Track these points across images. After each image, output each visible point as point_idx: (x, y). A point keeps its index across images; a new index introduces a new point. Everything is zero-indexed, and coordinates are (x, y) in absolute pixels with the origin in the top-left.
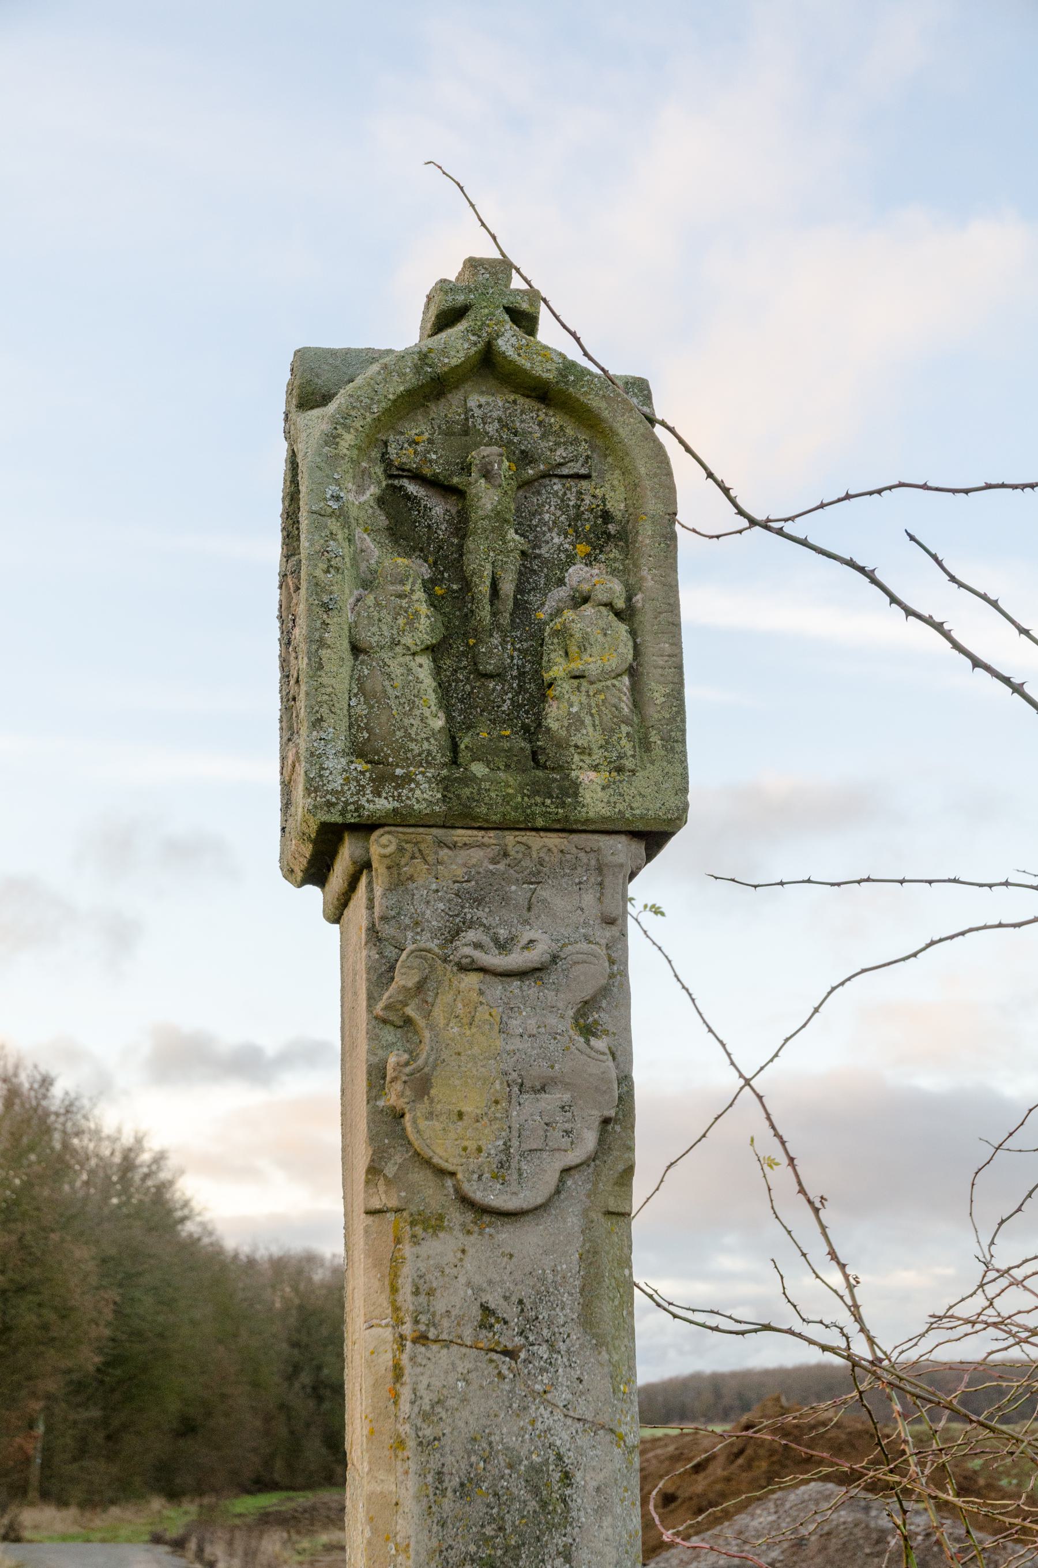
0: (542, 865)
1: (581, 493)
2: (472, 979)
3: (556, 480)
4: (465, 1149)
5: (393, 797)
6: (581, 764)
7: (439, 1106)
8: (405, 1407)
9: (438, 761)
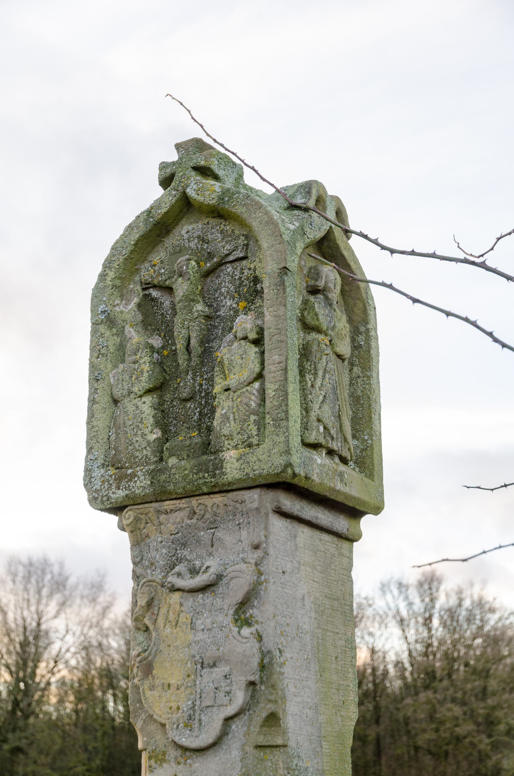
0: (216, 516)
1: (243, 269)
2: (176, 596)
3: (228, 265)
4: (171, 708)
5: (125, 488)
6: (228, 446)
7: (157, 681)
9: (152, 461)
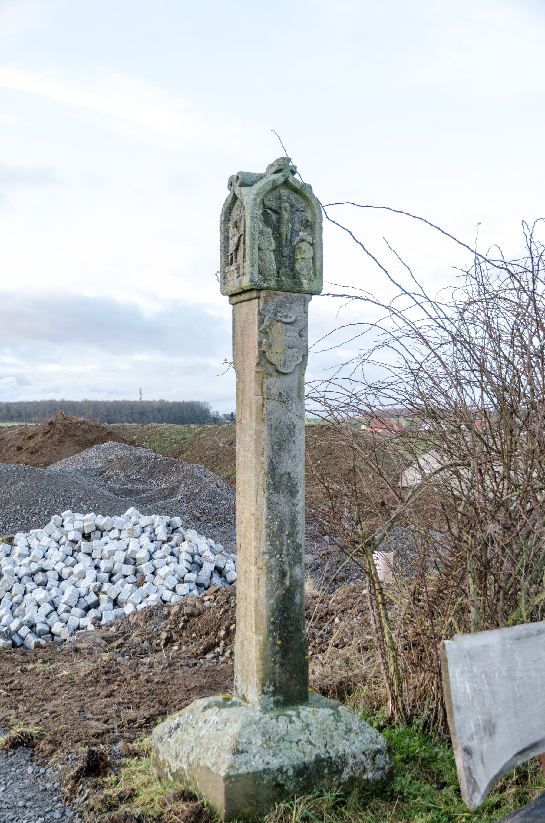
2: (280, 324)
8: (265, 412)
